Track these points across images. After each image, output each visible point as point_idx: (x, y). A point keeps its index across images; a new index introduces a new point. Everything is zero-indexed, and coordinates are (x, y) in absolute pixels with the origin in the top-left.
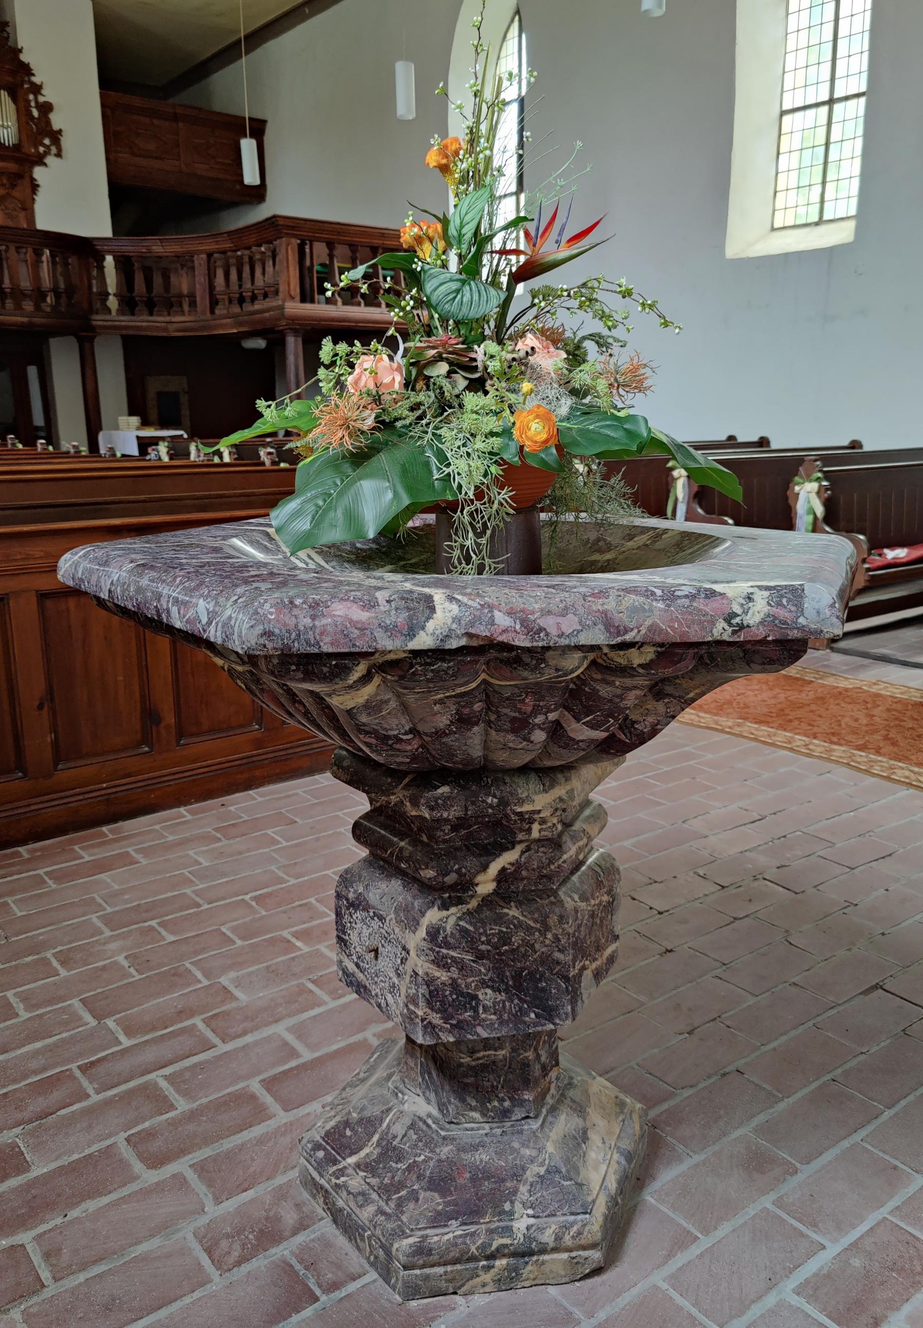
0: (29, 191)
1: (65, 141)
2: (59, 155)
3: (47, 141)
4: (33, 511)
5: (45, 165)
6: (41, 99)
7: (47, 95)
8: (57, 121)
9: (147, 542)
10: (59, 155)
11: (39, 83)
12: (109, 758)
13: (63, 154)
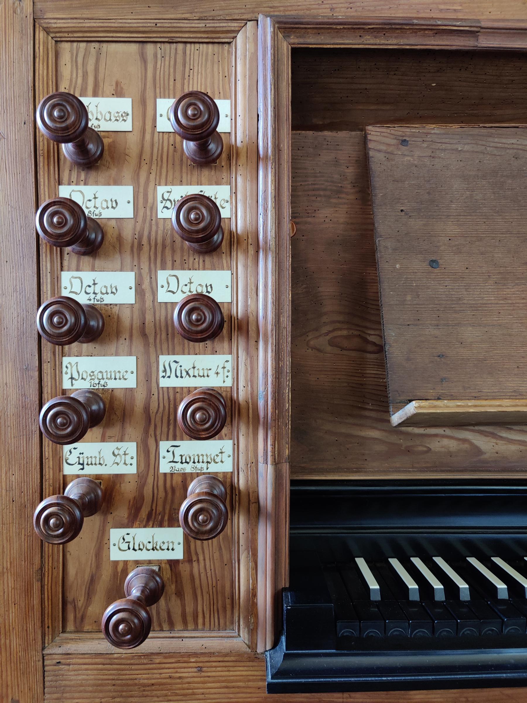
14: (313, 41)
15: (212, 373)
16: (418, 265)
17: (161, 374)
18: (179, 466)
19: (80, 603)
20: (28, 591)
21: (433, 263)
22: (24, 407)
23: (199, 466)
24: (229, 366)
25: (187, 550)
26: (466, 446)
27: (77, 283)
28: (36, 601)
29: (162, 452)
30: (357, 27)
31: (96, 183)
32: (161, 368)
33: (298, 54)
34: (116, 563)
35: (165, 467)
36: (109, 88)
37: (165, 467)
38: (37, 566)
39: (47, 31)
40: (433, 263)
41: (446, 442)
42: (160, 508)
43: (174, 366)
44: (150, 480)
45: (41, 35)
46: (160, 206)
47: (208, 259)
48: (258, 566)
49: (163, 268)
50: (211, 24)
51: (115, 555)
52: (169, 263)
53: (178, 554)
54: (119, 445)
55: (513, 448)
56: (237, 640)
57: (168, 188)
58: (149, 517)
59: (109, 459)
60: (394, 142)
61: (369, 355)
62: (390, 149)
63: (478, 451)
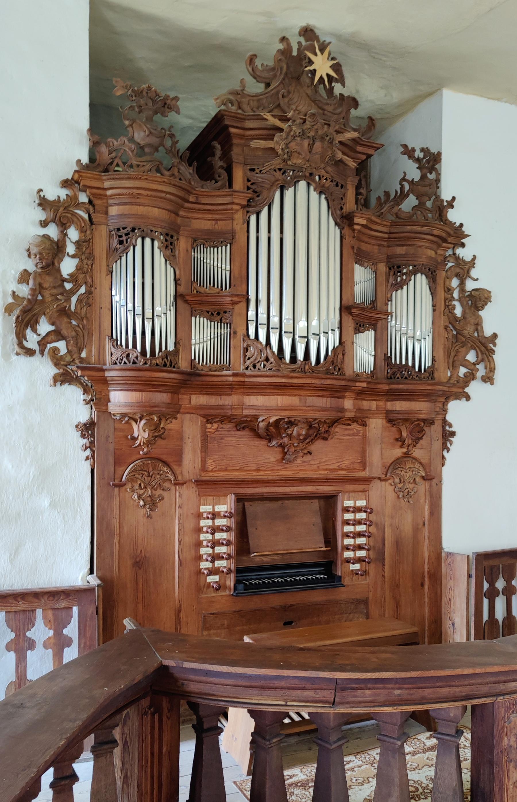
0: (438, 444)
1: (499, 357)
2: (488, 379)
3: (471, 357)
4: (260, 702)
5: (468, 398)
6: (470, 285)
7: (480, 278)
8: (491, 320)
9: (479, 691)
10: (488, 379)
11: (468, 258)
12: (311, 472)
13: (498, 376)
21: (256, 529)
33: (237, 499)
35: (216, 566)
40: (256, 529)
48: (231, 581)
53: (218, 580)
56: (228, 592)
63: (263, 560)
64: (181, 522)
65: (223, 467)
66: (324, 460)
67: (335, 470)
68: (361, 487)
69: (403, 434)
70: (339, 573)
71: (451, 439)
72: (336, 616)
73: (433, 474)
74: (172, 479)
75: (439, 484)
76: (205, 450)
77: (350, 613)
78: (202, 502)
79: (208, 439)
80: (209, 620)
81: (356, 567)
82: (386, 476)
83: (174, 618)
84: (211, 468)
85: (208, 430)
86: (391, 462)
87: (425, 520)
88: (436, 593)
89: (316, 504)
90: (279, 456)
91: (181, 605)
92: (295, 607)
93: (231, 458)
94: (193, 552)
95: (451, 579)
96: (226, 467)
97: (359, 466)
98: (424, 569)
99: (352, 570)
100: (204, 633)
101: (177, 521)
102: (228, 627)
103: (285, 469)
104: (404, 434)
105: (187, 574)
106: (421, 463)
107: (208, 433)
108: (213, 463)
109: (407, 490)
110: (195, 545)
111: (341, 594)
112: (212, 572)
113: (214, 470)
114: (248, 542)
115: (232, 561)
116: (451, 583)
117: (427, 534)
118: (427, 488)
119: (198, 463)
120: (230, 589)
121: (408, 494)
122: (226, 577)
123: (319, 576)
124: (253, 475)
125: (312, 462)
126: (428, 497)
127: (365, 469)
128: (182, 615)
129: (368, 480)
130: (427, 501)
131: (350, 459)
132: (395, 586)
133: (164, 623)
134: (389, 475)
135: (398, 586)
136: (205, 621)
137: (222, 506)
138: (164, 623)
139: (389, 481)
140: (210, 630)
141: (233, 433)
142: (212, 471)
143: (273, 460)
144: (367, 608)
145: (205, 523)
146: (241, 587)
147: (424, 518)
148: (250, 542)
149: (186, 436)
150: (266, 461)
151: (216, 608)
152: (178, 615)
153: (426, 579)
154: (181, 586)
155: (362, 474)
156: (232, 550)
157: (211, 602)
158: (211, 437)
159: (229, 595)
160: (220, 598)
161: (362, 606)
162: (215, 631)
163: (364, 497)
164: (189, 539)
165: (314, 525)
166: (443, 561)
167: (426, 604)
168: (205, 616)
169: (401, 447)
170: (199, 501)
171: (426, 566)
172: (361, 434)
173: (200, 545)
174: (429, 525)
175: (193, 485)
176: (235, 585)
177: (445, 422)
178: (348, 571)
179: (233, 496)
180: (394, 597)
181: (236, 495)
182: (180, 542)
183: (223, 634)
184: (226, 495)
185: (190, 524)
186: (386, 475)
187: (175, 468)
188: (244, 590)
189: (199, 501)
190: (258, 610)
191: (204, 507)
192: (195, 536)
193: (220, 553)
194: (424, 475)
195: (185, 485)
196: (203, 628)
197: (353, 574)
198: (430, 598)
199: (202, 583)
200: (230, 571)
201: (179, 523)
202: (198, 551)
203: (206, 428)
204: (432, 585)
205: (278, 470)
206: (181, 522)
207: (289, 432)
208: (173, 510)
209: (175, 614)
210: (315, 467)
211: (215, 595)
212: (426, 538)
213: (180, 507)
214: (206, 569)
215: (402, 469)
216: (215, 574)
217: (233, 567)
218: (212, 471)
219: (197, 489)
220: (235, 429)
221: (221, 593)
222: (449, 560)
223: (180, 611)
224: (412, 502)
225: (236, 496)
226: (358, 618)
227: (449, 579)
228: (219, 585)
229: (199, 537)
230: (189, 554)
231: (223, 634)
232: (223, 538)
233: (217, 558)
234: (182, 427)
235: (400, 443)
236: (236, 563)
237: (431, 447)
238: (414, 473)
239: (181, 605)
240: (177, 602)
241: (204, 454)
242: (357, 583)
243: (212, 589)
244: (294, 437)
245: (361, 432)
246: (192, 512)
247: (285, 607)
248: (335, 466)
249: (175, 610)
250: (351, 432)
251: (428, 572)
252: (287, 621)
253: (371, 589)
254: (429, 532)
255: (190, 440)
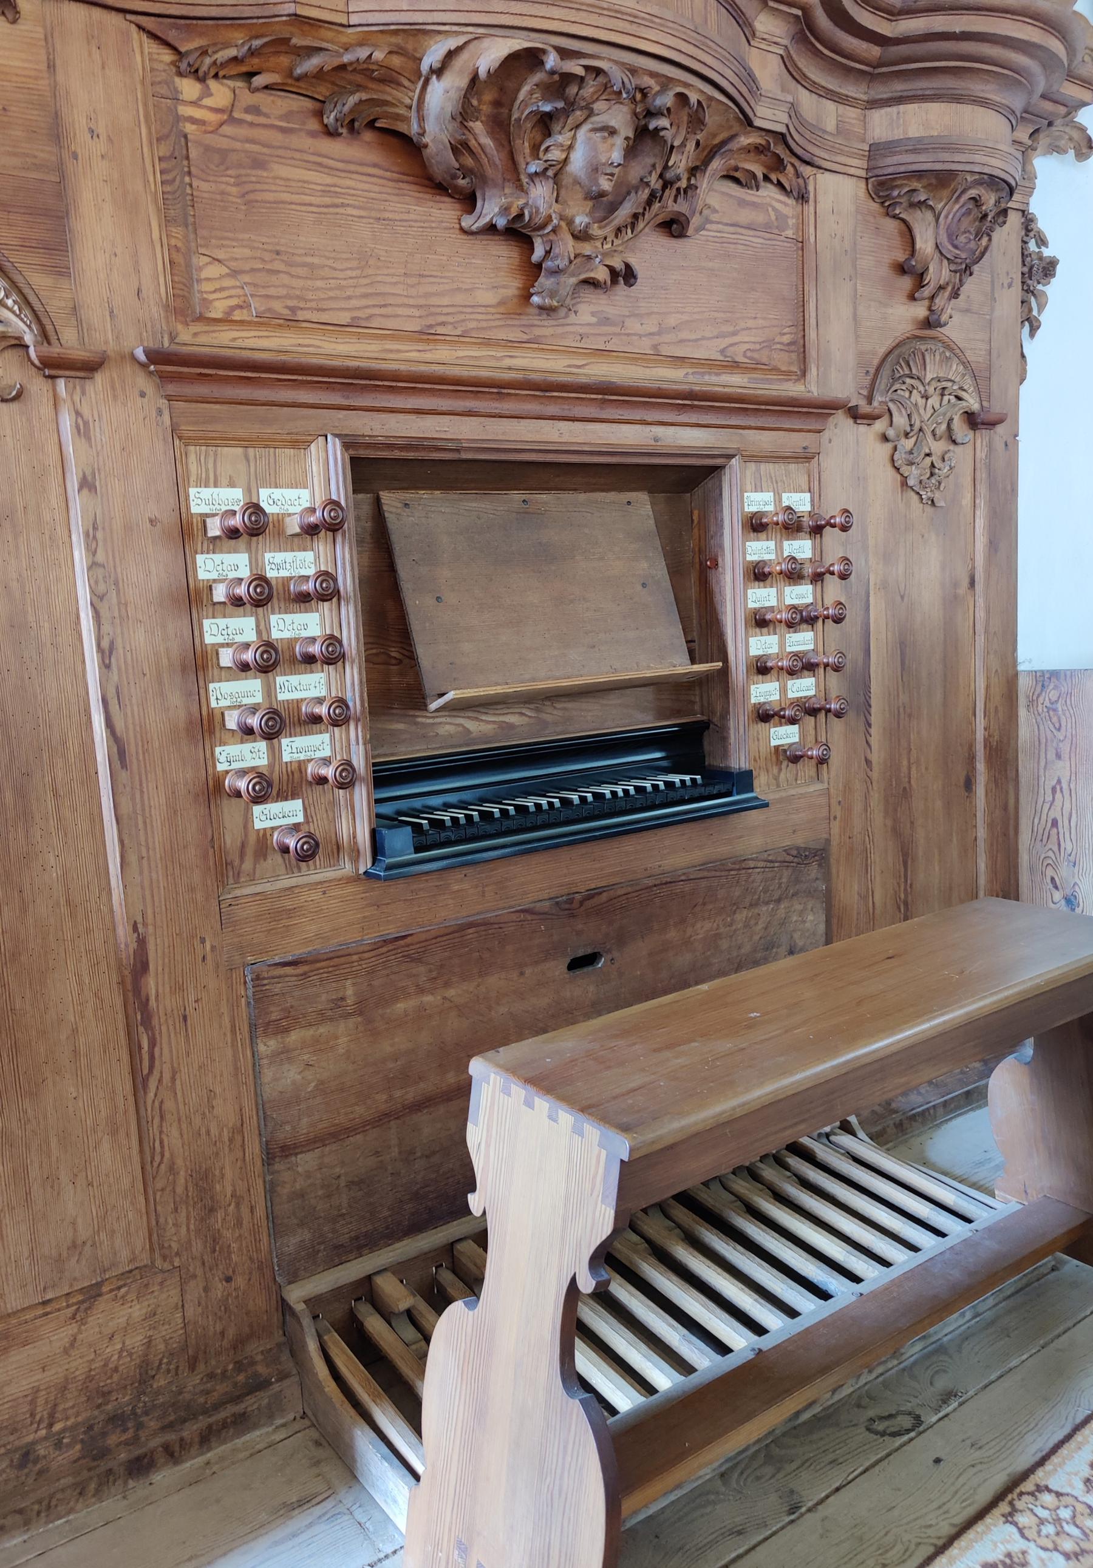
0: (1009, 299)
14: (363, 453)
15: (312, 687)
16: (430, 601)
17: (278, 690)
18: (295, 755)
19: (236, 863)
20: (205, 857)
21: (438, 599)
22: (191, 722)
23: (308, 754)
24: (323, 681)
25: (306, 816)
26: (461, 728)
27: (214, 627)
28: (211, 863)
29: (284, 747)
30: (391, 447)
31: (221, 552)
32: (278, 686)
33: (353, 459)
34: (258, 830)
35: (286, 758)
36: (225, 481)
37: (286, 758)
38: (210, 837)
39: (180, 438)
40: (438, 599)
41: (447, 727)
42: (285, 788)
43: (286, 684)
44: (277, 768)
45: (177, 442)
46: (268, 568)
47: (302, 605)
48: (355, 818)
49: (273, 613)
50: (295, 437)
51: (258, 825)
52: (277, 610)
53: (300, 818)
54: (254, 744)
55: (490, 726)
56: (347, 868)
57: (272, 554)
58: (278, 795)
59: (248, 756)
60: (400, 505)
61: (392, 667)
62: (399, 511)
63: (469, 731)
64: (100, 557)
65: (278, 306)
66: (672, 321)
67: (709, 365)
68: (795, 442)
69: (919, 244)
70: (738, 761)
71: (1040, 287)
72: (738, 917)
73: (996, 408)
74: (28, 339)
75: (1011, 444)
76: (180, 208)
77: (779, 901)
78: (193, 467)
79: (193, 153)
80: (277, 988)
81: (785, 735)
82: (870, 402)
83: (119, 1002)
84: (217, 311)
85: (185, 111)
86: (882, 351)
87: (974, 568)
88: (1005, 808)
89: (641, 508)
90: (512, 286)
91: (142, 942)
92: (604, 897)
93: (311, 266)
94: (176, 699)
95: (1059, 756)
96: (293, 309)
97: (785, 356)
98: (974, 732)
99: (777, 748)
100: (262, 1048)
101: (79, 555)
102: (362, 1008)
103: (534, 343)
104: (925, 243)
105: (157, 800)
106: (966, 364)
107: (189, 128)
108: (228, 282)
109: (928, 460)
110: (184, 669)
111: (751, 835)
112: (268, 787)
113: (237, 316)
114: (410, 657)
115: (355, 732)
116: (1062, 770)
117: (981, 614)
118: (981, 454)
119: (155, 283)
120: (355, 854)
121: (932, 474)
122: (334, 803)
123: (530, 802)
124: (407, 357)
125: (634, 326)
126: (982, 489)
127: (804, 373)
128: (151, 984)
129: (820, 410)
130: (981, 502)
131: (756, 328)
132: (899, 796)
133: (75, 1031)
134: (878, 398)
135: (906, 793)
136: (261, 1000)
137: (291, 494)
138: (75, 1031)
139: (880, 426)
140: (286, 1030)
141: (307, 143)
142: (226, 321)
143: (488, 297)
144: (827, 877)
145: (230, 632)
146: (400, 841)
147: (973, 560)
148: (421, 651)
149: (77, 120)
150: (459, 299)
151: (305, 937)
152: (137, 990)
153: (981, 766)
154: (133, 858)
155: (794, 389)
156: (351, 682)
157: (279, 913)
158: (208, 149)
159: (356, 879)
160: (316, 896)
161: (814, 871)
162: (309, 1033)
163: (803, 480)
164: (148, 640)
165: (644, 585)
166: (1022, 701)
167: (981, 846)
168: (258, 978)
169: (912, 298)
170: (178, 462)
171: (980, 722)
172: (790, 233)
173: (205, 668)
174: (987, 585)
175: (142, 381)
176: (374, 833)
177: (1028, 223)
178: (763, 750)
179: (335, 447)
180: (896, 832)
181: (348, 444)
182: (106, 654)
183: (343, 1040)
184: (300, 443)
185: (148, 571)
186: (870, 399)
187: (38, 281)
188: (417, 850)
189: (178, 462)
190: (471, 925)
191: (206, 493)
192: (178, 626)
193: (299, 702)
194: (975, 407)
195: (99, 377)
196: (253, 1027)
197: (779, 763)
198: (991, 826)
199: (231, 839)
200: (346, 781)
201: (93, 566)
202: (200, 695)
203: (176, 98)
204: (996, 781)
205: (509, 344)
206: (100, 557)
207: (556, 155)
208: (55, 500)
209: (122, 983)
210: (644, 346)
211: (293, 882)
212: (980, 628)
213: (86, 484)
214: (242, 773)
215: (912, 381)
216: (282, 796)
217: (359, 762)
218: (226, 321)
219: (163, 403)
220: (313, 125)
221: (318, 873)
222: (1045, 699)
223: (141, 966)
224: (942, 504)
225: (346, 446)
226: (801, 913)
227: (1051, 755)
228: (310, 836)
229: (195, 630)
230: (160, 712)
231: (343, 1040)
232: (305, 634)
233: (290, 720)
234: (51, 66)
235: (906, 283)
236: (374, 740)
237: (992, 309)
238: (946, 398)
239: (142, 942)
240: (123, 932)
241: (177, 231)
242: (793, 792)
243: (278, 858)
244: (577, 182)
245: (791, 222)
246: (152, 510)
247: (571, 901)
248: (709, 351)
249: (120, 967)
250: (760, 218)
251: (985, 740)
252: (581, 953)
253: (837, 811)
254: (988, 611)
255: (99, 147)
